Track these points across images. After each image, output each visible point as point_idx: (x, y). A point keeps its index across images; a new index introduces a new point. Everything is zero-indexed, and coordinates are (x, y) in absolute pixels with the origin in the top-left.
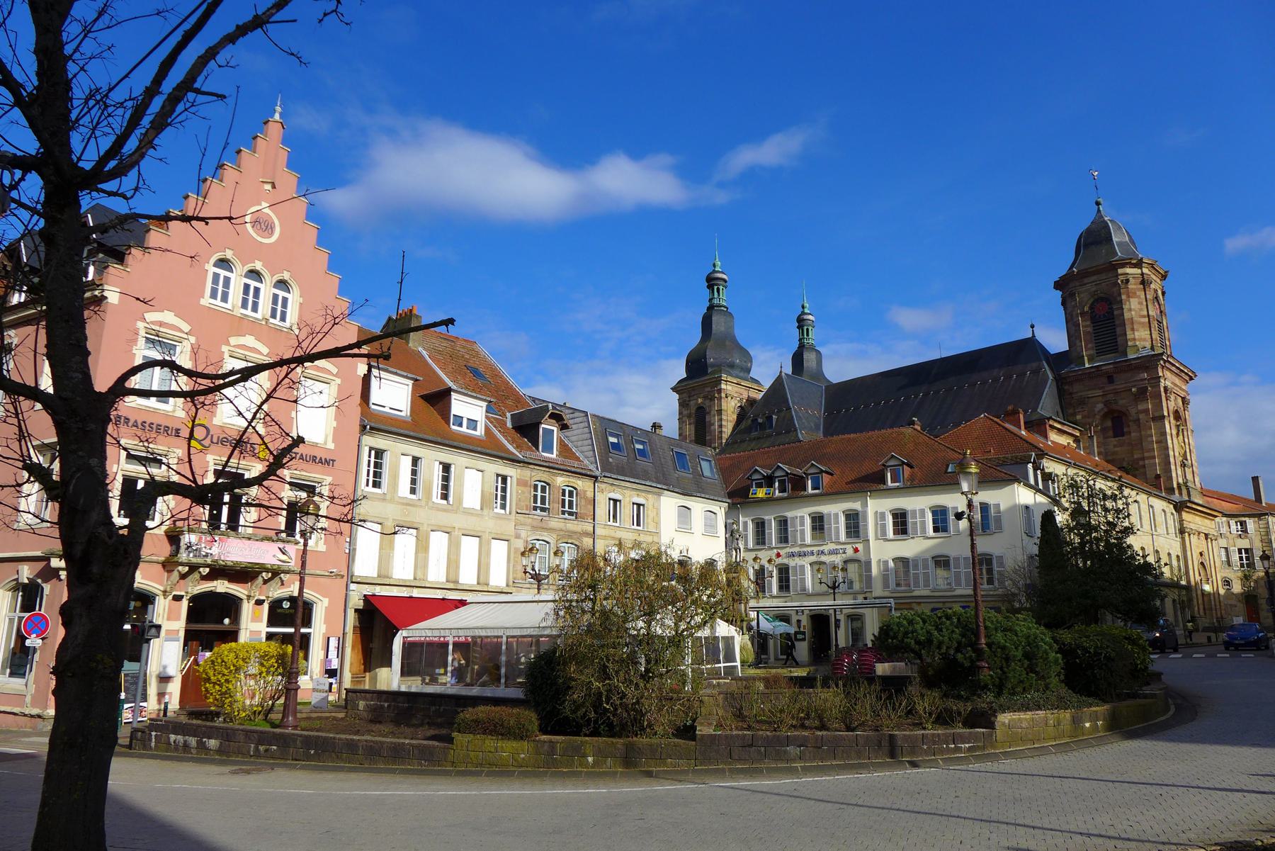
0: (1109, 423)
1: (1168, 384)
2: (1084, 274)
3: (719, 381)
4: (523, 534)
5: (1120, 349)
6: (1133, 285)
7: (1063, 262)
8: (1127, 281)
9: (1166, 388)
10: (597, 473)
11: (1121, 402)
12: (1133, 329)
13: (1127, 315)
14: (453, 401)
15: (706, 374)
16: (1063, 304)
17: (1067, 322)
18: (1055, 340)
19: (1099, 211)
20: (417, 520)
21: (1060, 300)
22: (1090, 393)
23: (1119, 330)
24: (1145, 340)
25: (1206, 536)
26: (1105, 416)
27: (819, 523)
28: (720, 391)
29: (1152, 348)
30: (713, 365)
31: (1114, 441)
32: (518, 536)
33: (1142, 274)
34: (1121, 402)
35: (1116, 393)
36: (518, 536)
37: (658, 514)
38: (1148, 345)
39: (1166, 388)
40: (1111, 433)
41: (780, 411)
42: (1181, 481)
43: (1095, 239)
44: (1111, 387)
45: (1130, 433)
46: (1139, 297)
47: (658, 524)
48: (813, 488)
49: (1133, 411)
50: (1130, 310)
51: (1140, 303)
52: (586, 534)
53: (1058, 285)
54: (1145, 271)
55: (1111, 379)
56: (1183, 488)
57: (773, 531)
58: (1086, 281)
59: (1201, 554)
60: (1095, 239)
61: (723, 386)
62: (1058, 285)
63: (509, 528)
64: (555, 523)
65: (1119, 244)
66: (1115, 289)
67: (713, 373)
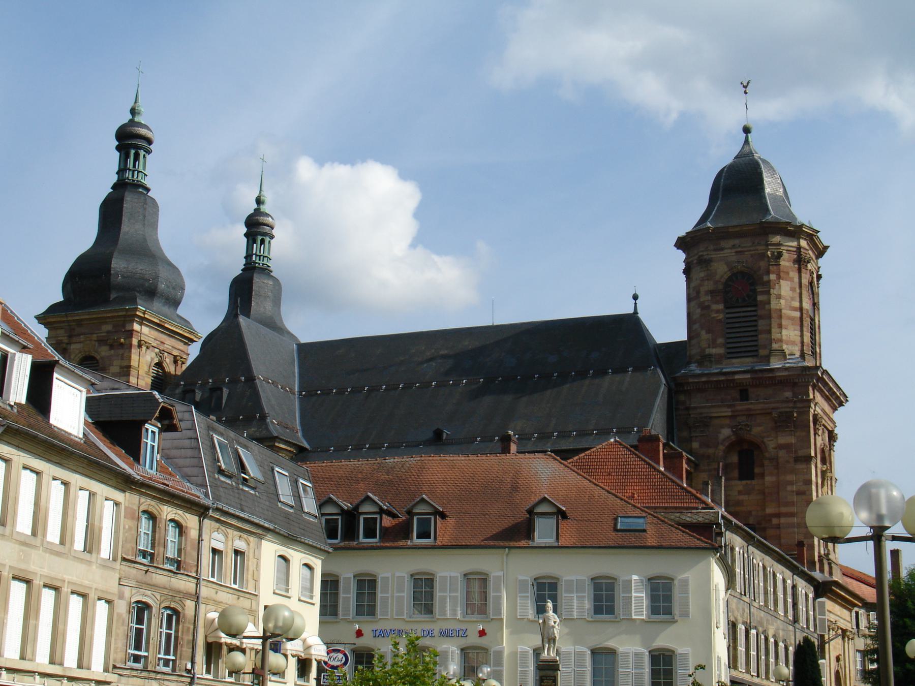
0: (734, 459)
1: (818, 410)
2: (720, 235)
3: (131, 317)
4: (127, 592)
5: (762, 352)
6: (786, 262)
7: (691, 210)
8: (780, 255)
9: (815, 416)
10: (208, 502)
11: (756, 430)
12: (780, 326)
13: (774, 305)
14: (55, 381)
15: (106, 301)
16: (687, 272)
17: (689, 300)
18: (667, 323)
19: (747, 142)
20: (32, 568)
21: (683, 266)
22: (715, 412)
23: (761, 324)
24: (793, 343)
25: (844, 631)
26: (730, 449)
27: (424, 591)
28: (130, 333)
29: (803, 356)
30: (121, 288)
31: (739, 485)
32: (121, 597)
33: (799, 248)
34: (756, 430)
35: (750, 415)
36: (121, 597)
37: (258, 565)
38: (797, 351)
39: (815, 416)
40: (736, 473)
41: (234, 381)
42: (822, 552)
43: (740, 182)
44: (741, 406)
45: (762, 475)
46: (792, 280)
47: (256, 587)
48: (366, 536)
49: (771, 444)
50: (779, 297)
51: (793, 289)
52: (187, 595)
53: (682, 243)
54: (803, 243)
55: (744, 395)
56: (825, 562)
57: (348, 596)
58: (723, 244)
59: (838, 659)
60: (740, 182)
61: (136, 327)
62: (682, 243)
63: (112, 586)
64: (159, 578)
65: (769, 194)
66: (763, 264)
67: (122, 300)
